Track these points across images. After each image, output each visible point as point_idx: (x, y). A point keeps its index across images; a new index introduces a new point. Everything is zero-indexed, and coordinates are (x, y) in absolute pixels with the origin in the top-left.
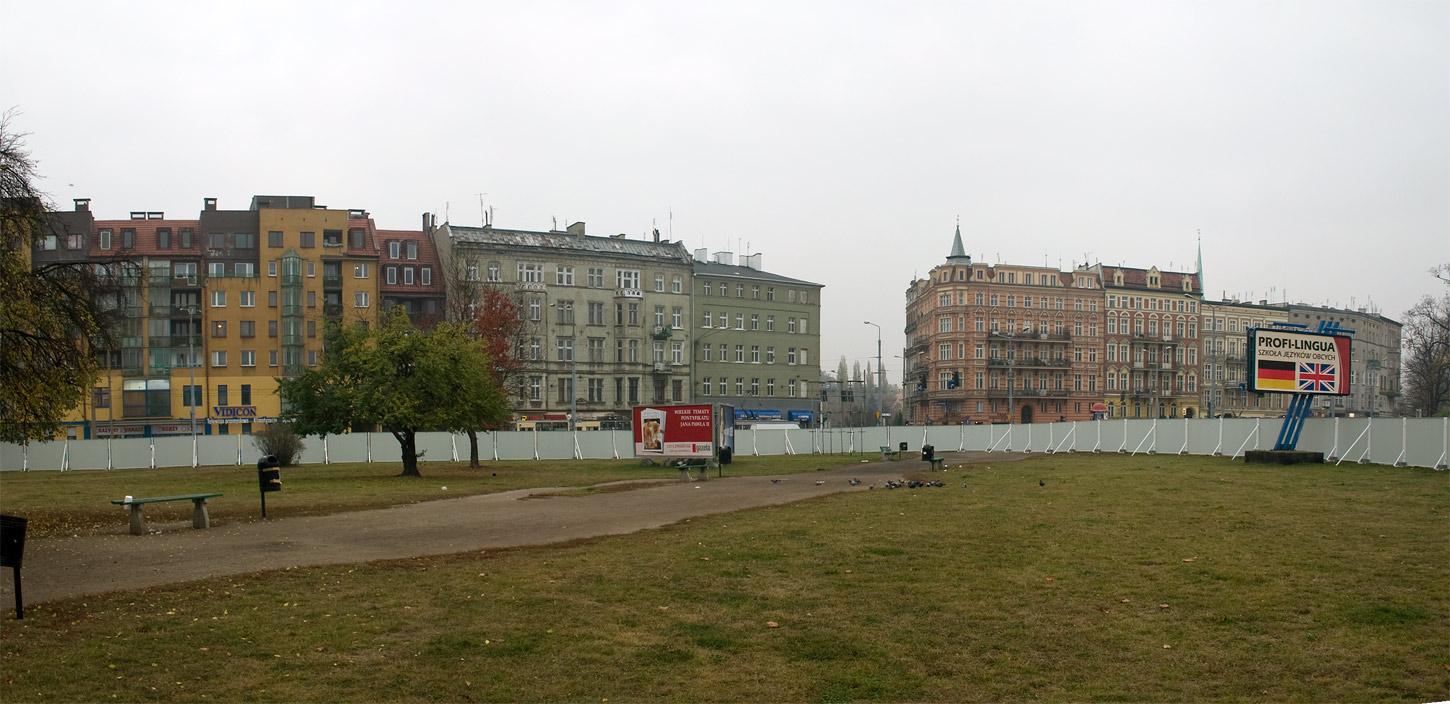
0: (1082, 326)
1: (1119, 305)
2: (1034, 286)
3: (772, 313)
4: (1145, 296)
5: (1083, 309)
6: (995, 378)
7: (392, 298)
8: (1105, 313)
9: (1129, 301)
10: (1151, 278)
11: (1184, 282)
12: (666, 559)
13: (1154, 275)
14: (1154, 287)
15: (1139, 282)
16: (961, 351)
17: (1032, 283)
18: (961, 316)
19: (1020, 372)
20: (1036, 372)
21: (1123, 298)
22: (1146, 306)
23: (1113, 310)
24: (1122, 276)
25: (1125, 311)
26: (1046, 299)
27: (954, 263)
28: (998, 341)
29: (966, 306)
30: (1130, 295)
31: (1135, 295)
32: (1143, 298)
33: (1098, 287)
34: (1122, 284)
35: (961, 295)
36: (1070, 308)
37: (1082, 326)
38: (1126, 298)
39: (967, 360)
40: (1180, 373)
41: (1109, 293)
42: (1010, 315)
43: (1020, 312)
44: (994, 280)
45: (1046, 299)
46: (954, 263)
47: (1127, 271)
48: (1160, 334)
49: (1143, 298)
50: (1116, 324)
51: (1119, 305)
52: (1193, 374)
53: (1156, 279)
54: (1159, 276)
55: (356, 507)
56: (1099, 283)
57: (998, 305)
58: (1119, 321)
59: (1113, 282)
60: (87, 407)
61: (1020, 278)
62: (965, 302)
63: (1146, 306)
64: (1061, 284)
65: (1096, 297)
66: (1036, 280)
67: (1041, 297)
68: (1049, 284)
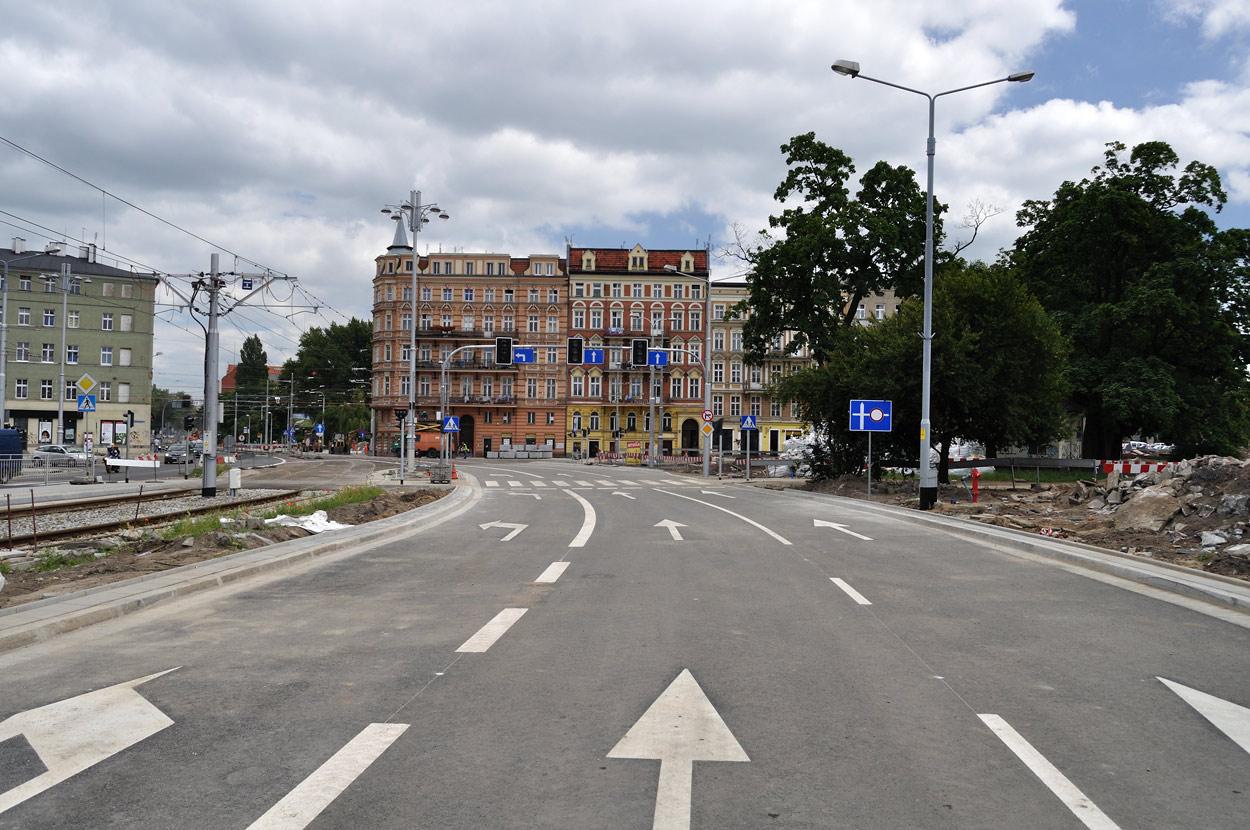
0: (538, 322)
1: (588, 293)
2: (476, 276)
3: (109, 310)
4: (624, 281)
5: (539, 301)
6: (488, 385)
7: (466, 335)
8: (569, 304)
9: (602, 288)
10: (635, 259)
11: (584, 258)
12: (788, 749)
13: (638, 255)
14: (638, 269)
15: (618, 264)
16: (388, 353)
17: (474, 273)
18: (389, 313)
19: (456, 376)
20: (477, 377)
21: (595, 285)
22: (648, 293)
23: (579, 300)
24: (593, 258)
25: (597, 301)
26: (556, 292)
27: (395, 253)
28: (430, 341)
29: (394, 302)
30: (604, 280)
31: (610, 280)
32: (664, 285)
33: (560, 273)
34: (646, 268)
35: (390, 290)
36: (521, 300)
37: (538, 322)
38: (599, 286)
39: (393, 363)
40: (676, 375)
41: (574, 280)
42: (531, 311)
43: (457, 306)
44: (426, 271)
45: (556, 292)
46: (395, 253)
47: (597, 251)
48: (647, 326)
49: (623, 284)
50: (584, 317)
51: (588, 293)
52: (694, 375)
53: (642, 259)
54: (646, 256)
55: (197, 589)
56: (564, 270)
57: (473, 300)
58: (687, 315)
59: (627, 268)
60: (133, 506)
61: (459, 268)
62: (394, 298)
63: (648, 293)
64: (511, 273)
65: (546, 285)
66: (480, 268)
67: (548, 289)
68: (496, 272)
